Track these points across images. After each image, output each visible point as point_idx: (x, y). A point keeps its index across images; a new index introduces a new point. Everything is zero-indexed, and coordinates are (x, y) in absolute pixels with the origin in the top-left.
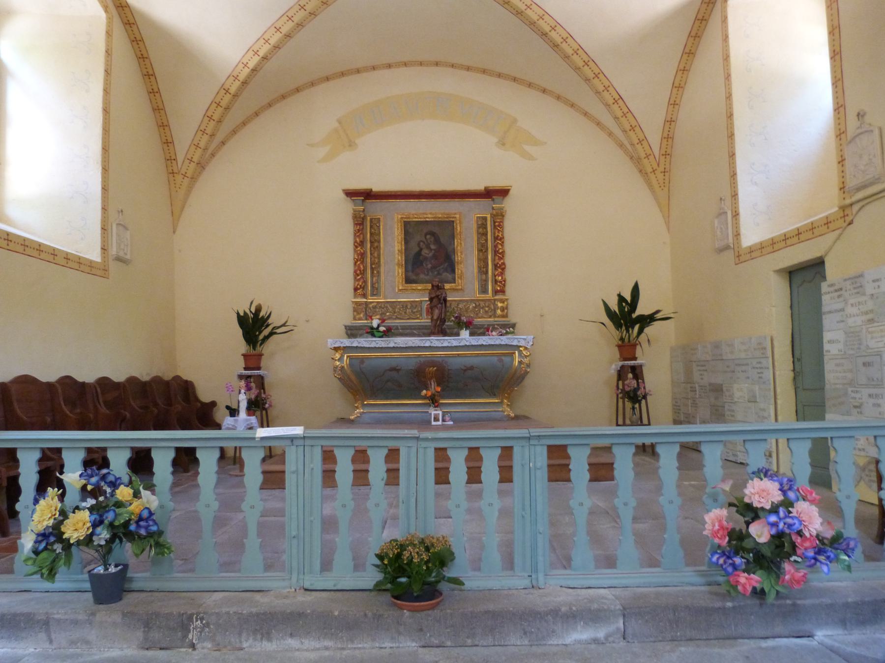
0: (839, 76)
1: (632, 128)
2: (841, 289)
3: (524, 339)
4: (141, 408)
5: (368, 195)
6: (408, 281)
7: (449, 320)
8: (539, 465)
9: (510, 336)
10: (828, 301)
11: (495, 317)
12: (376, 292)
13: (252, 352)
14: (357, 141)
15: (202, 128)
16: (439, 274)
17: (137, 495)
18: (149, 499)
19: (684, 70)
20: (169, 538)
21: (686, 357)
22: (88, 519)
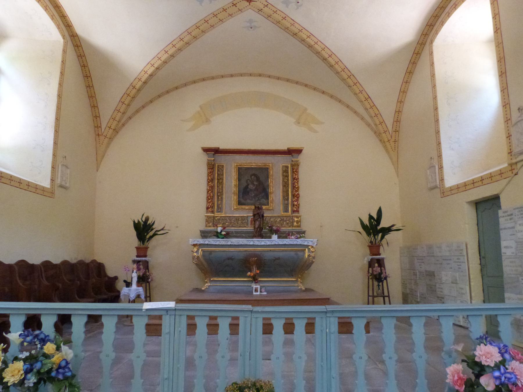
0: (505, 85)
1: (376, 115)
2: (512, 215)
3: (312, 241)
4: (70, 281)
5: (217, 151)
6: (240, 203)
8: (332, 331)
9: (302, 239)
10: (503, 222)
11: (293, 227)
12: (220, 209)
13: (142, 246)
15: (118, 109)
16: (259, 200)
17: (58, 349)
18: (67, 352)
19: (406, 83)
20: (79, 380)
21: (410, 253)
22: (22, 368)
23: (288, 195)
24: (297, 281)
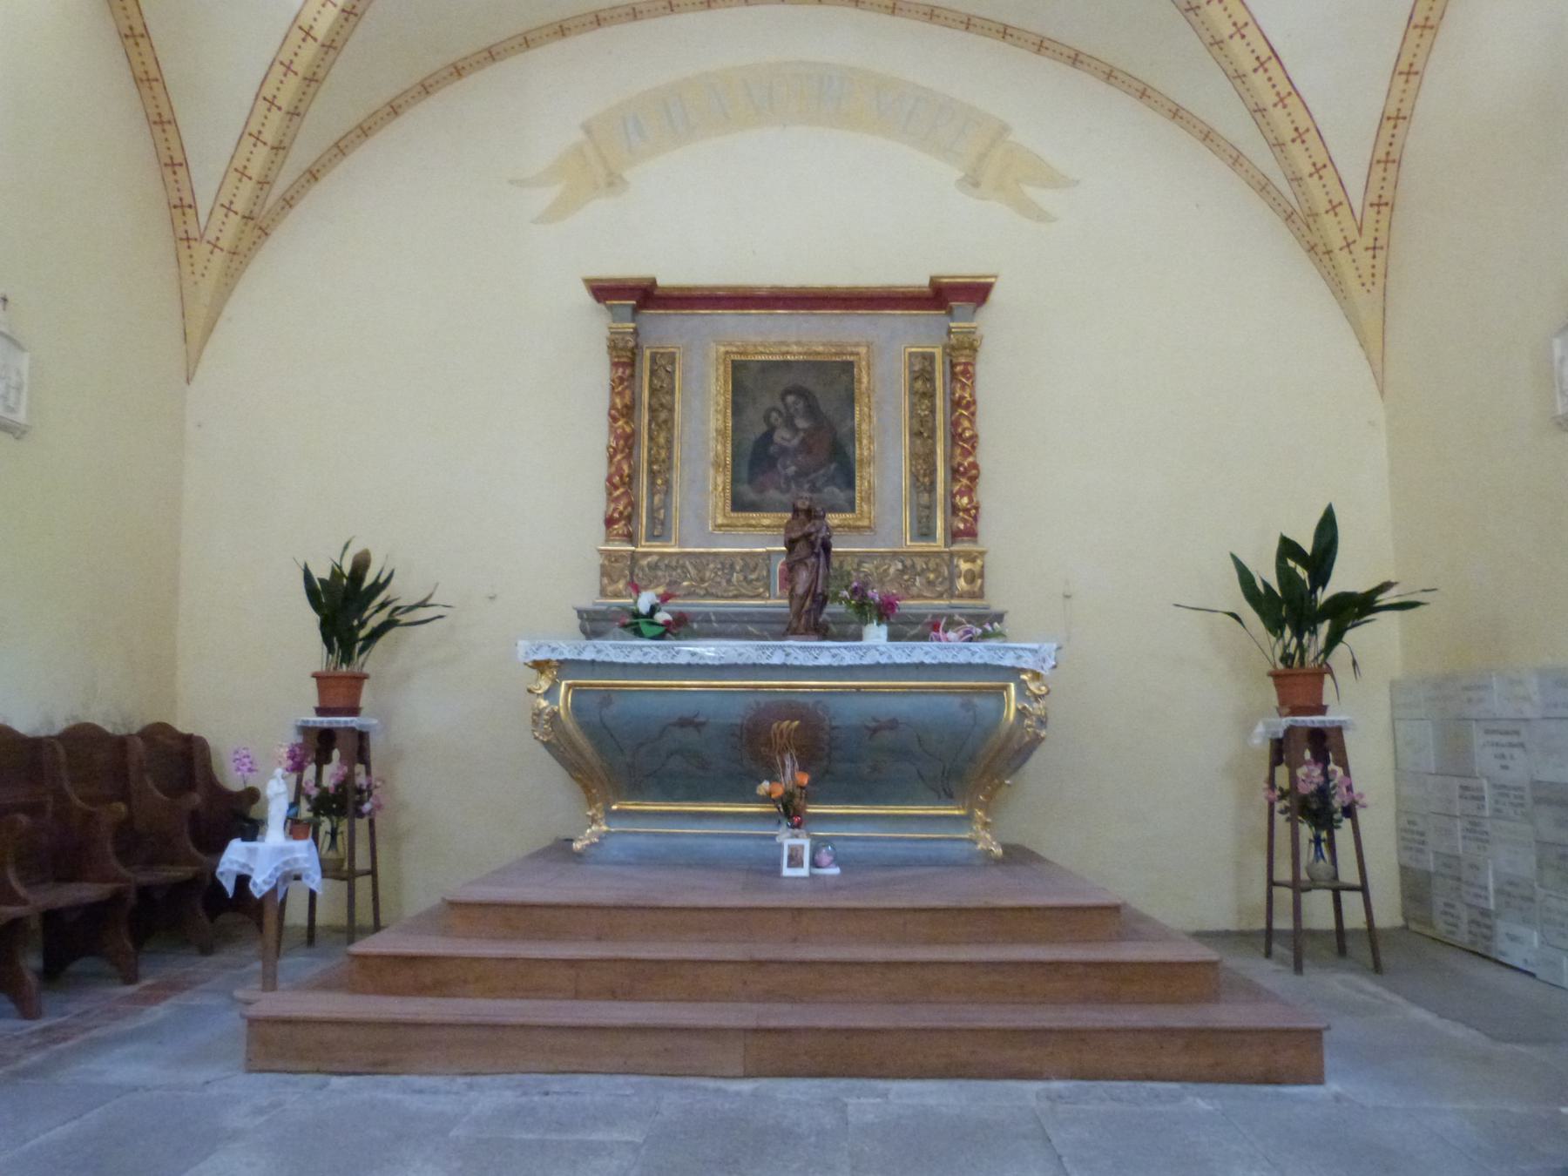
1: (1299, 135)
5: (647, 296)
7: (836, 598)
9: (993, 643)
11: (952, 596)
12: (659, 529)
14: (627, 175)
23: (932, 472)
24: (969, 818)
